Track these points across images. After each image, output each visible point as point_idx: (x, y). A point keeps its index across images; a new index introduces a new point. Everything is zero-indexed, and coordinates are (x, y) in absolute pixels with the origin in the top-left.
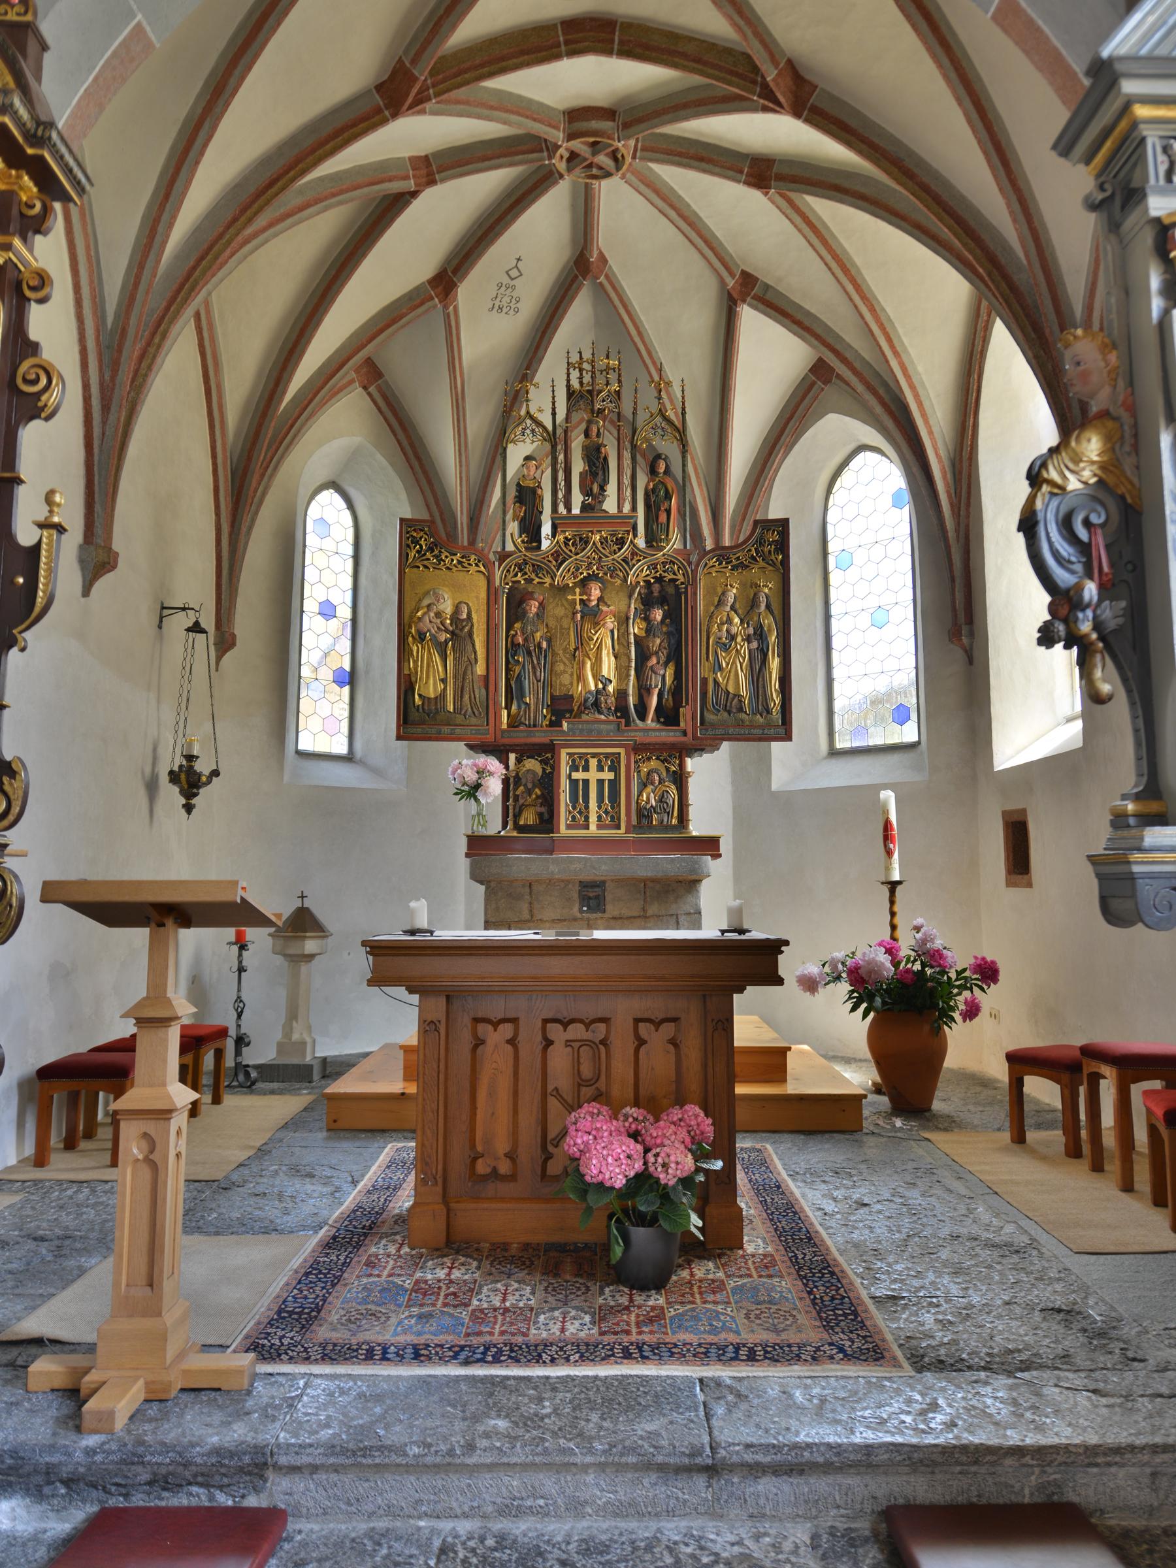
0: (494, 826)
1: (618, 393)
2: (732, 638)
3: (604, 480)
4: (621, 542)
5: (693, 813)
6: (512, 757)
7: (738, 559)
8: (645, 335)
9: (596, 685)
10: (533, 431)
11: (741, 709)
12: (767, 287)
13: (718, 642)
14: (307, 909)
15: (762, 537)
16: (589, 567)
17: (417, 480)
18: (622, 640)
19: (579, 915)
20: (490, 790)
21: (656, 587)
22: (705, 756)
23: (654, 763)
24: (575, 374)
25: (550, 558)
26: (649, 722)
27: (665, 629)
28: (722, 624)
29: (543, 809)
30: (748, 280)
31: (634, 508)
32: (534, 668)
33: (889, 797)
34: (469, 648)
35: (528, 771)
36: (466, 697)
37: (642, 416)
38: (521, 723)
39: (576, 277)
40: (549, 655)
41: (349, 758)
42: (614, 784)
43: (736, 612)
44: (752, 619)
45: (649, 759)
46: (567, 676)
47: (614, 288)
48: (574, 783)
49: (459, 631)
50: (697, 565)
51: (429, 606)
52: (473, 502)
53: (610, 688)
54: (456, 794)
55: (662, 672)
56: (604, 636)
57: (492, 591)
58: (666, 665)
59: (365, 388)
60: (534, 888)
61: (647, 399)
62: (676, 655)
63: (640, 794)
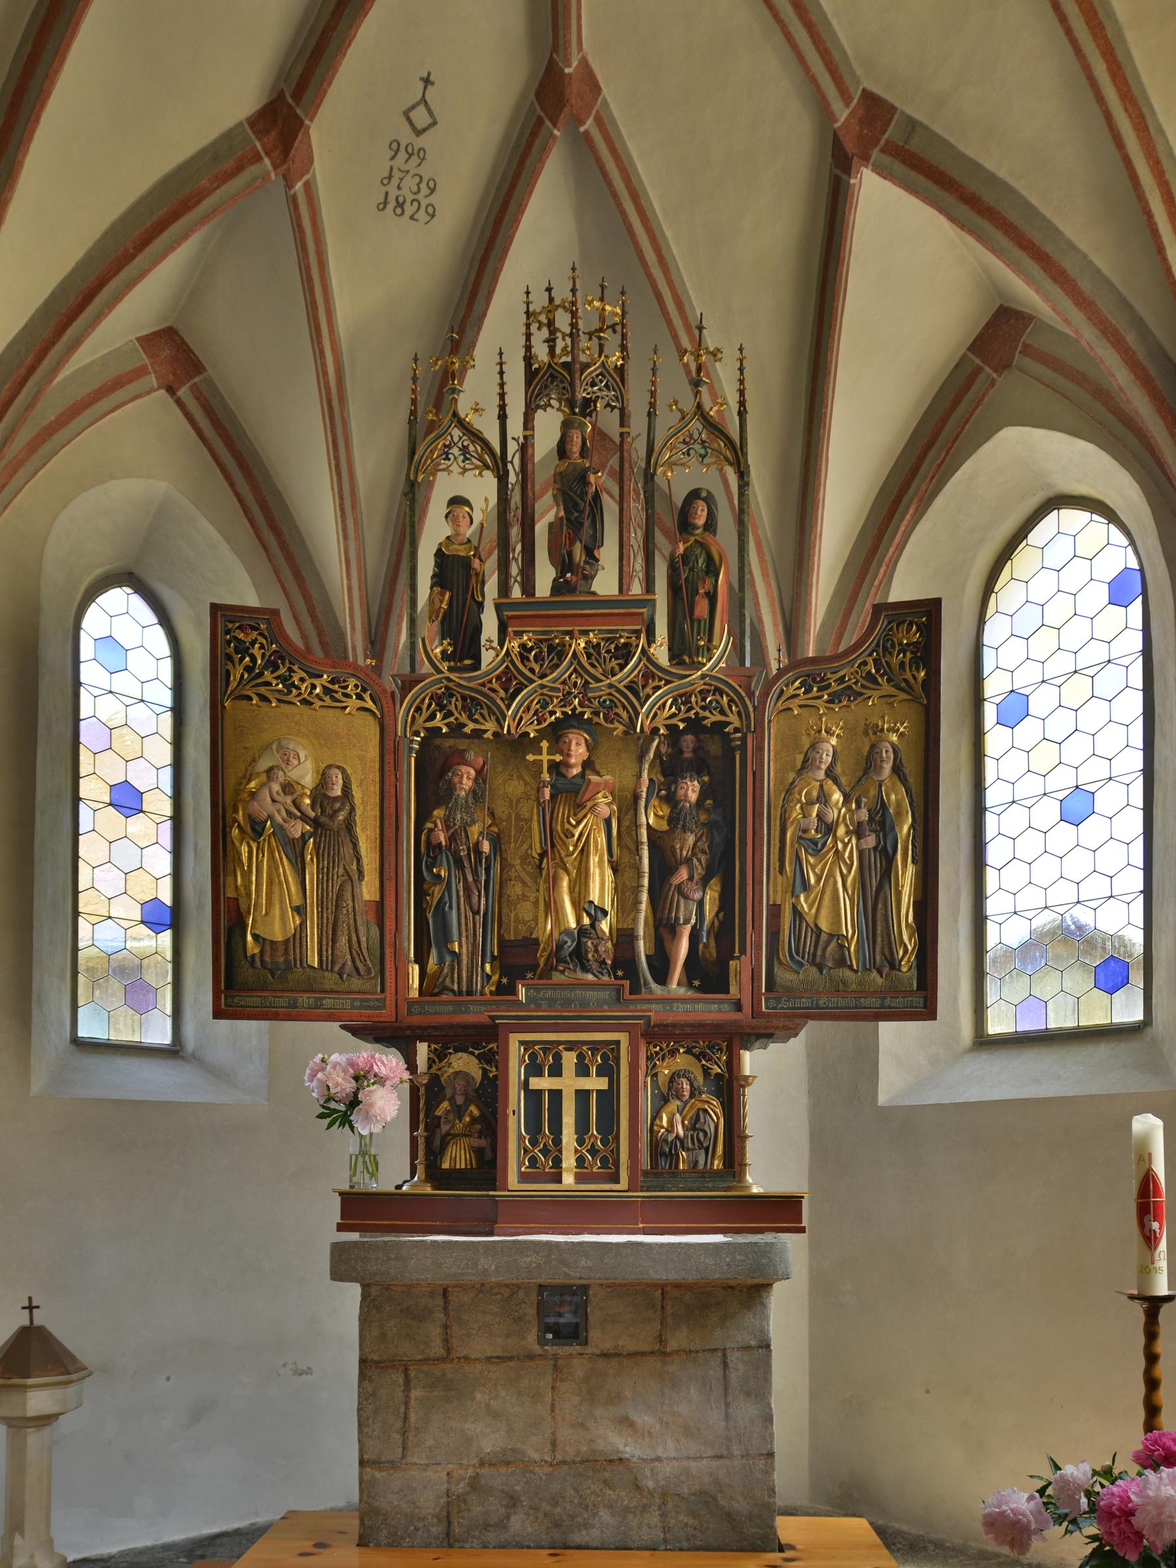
0: (395, 1172)
1: (621, 371)
2: (829, 829)
3: (594, 536)
4: (624, 653)
5: (753, 1152)
6: (422, 1050)
7: (841, 680)
8: (673, 272)
9: (579, 919)
10: (464, 449)
11: (842, 962)
12: (913, 125)
13: (802, 836)
14: (41, 1330)
15: (887, 636)
16: (565, 702)
17: (276, 571)
18: (628, 841)
19: (537, 1349)
20: (376, 1110)
21: (689, 741)
22: (773, 1047)
23: (682, 1061)
24: (539, 337)
25: (495, 685)
26: (674, 986)
27: (703, 817)
28: (810, 803)
29: (483, 1142)
30: (875, 109)
31: (649, 586)
32: (467, 889)
33: (1149, 1126)
34: (347, 850)
35: (457, 1073)
36: (343, 940)
37: (666, 420)
38: (446, 989)
39: (540, 122)
40: (497, 868)
41: (174, 1051)
42: (608, 1099)
43: (836, 781)
44: (865, 793)
45: (673, 1053)
46: (528, 905)
47: (613, 151)
48: (534, 1097)
49: (328, 819)
50: (765, 694)
51: (269, 771)
52: (375, 610)
53: (605, 926)
54: (321, 1116)
55: (697, 896)
56: (592, 830)
57: (389, 745)
58: (705, 882)
59: (171, 390)
60: (453, 1298)
61: (674, 389)
62: (723, 865)
63: (656, 1115)
